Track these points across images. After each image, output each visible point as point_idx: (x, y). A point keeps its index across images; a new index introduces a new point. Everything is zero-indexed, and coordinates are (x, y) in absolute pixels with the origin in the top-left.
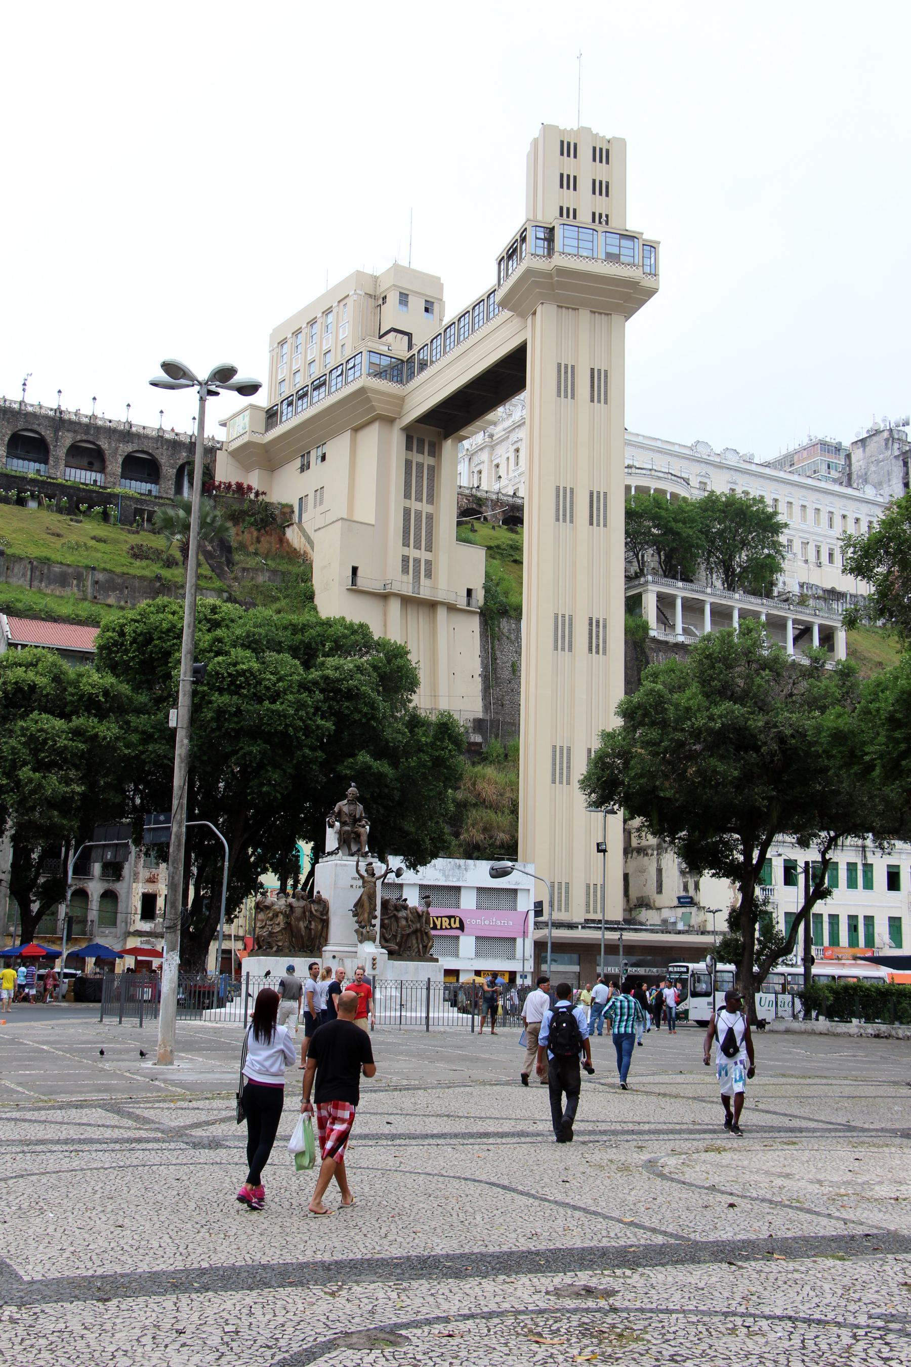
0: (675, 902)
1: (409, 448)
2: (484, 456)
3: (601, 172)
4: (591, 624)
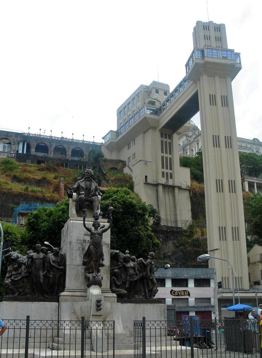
1: (162, 137)
3: (218, 34)
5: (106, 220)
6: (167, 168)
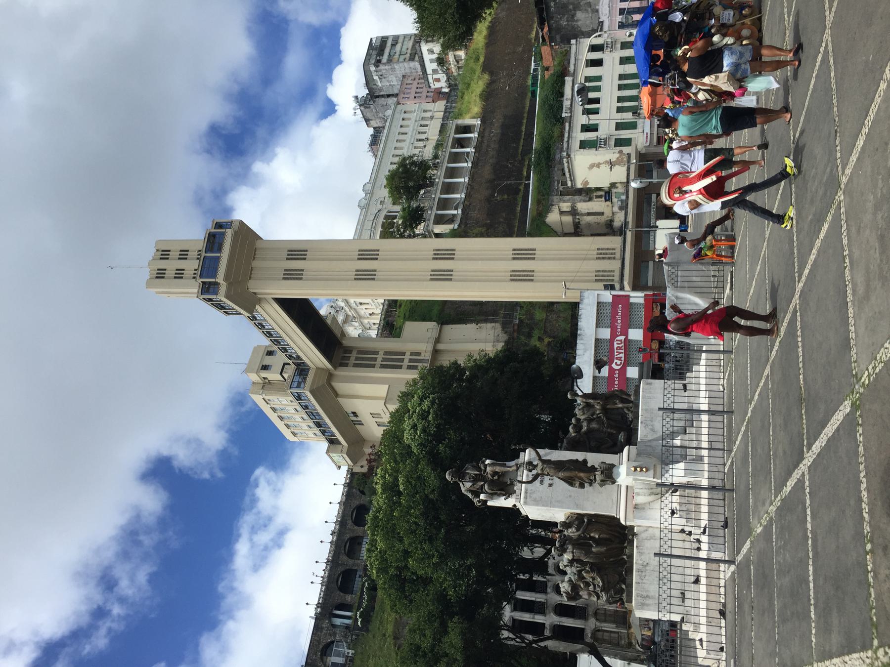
0: (609, 203)
1: (346, 365)
2: (366, 321)
4: (437, 259)
5: (522, 454)
6: (384, 360)
